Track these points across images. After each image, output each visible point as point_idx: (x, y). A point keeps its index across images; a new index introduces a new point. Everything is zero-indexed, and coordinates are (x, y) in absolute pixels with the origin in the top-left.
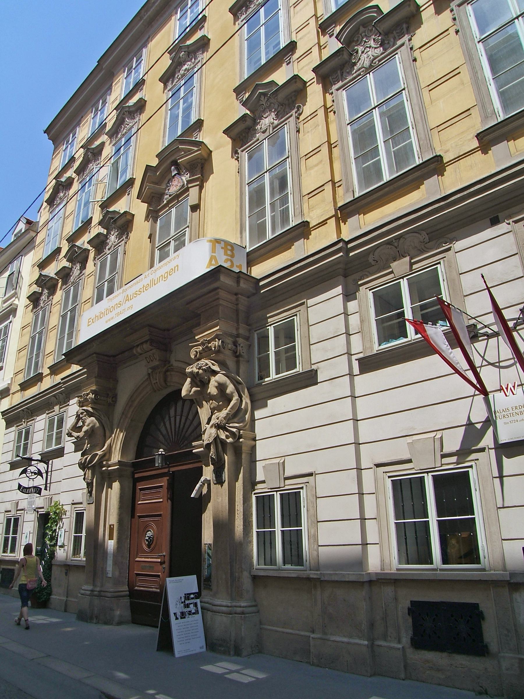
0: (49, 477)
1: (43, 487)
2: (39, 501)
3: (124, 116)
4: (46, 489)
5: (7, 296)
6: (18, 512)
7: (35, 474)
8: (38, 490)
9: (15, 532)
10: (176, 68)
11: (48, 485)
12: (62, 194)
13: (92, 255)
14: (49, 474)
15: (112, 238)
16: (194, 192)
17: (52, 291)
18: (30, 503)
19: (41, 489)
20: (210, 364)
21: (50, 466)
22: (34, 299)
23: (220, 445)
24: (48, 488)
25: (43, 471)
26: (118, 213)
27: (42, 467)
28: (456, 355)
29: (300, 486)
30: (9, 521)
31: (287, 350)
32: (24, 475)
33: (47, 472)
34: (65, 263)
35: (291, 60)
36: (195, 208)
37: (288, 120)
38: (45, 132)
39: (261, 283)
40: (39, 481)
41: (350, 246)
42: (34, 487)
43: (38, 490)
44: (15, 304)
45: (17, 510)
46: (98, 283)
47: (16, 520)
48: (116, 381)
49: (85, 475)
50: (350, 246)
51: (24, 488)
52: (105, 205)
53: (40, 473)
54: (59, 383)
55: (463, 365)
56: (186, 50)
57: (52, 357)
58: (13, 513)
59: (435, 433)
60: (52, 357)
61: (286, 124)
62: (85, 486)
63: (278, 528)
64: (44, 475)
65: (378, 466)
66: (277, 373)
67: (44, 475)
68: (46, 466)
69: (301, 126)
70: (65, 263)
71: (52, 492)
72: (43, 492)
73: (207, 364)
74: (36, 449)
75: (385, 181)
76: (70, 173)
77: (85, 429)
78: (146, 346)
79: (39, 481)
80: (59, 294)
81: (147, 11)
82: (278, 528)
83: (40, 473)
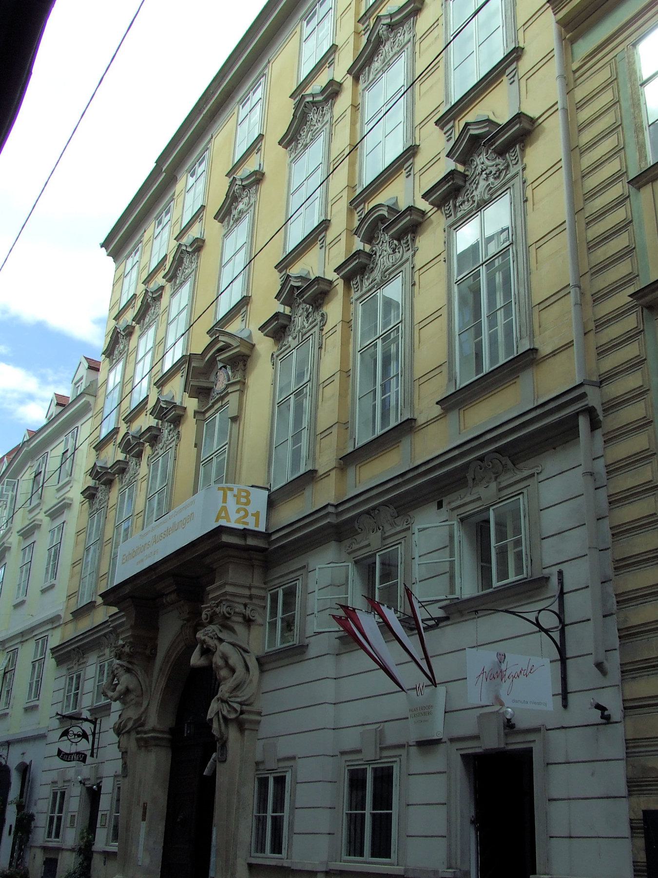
0: (96, 740)
1: (88, 753)
2: (85, 771)
3: (182, 256)
4: (92, 755)
5: (60, 485)
6: (386, 753)
7: (79, 736)
8: (82, 757)
10: (231, 204)
11: (95, 751)
14: (97, 736)
15: (299, 321)
16: (233, 399)
17: (109, 483)
18: (78, 773)
19: (86, 756)
20: (217, 632)
21: (98, 726)
22: (90, 494)
23: (222, 721)
25: (89, 732)
26: (307, 279)
27: (87, 727)
28: (412, 643)
29: (394, 759)
32: (65, 738)
33: (94, 734)
34: (152, 421)
35: (412, 172)
36: (235, 419)
37: (512, 182)
39: (274, 537)
40: (84, 746)
42: (78, 753)
43: (82, 757)
44: (68, 499)
45: (382, 749)
46: (458, 275)
47: (63, 794)
48: (156, 629)
49: (119, 742)
51: (66, 754)
52: (283, 265)
53: (84, 735)
54: (107, 621)
55: (418, 654)
56: (388, 21)
57: (105, 581)
58: (60, 785)
59: (378, 725)
60: (105, 581)
61: (509, 188)
62: (120, 755)
63: (368, 811)
64: (91, 738)
65: (343, 753)
66: (282, 642)
67: (91, 738)
68: (92, 726)
69: (529, 193)
70: (152, 421)
71: (99, 760)
73: (214, 631)
74: (87, 701)
76: (159, 280)
77: (118, 688)
78: (173, 597)
79: (84, 746)
80: (114, 493)
81: (206, 103)
82: (368, 811)
83: (84, 735)
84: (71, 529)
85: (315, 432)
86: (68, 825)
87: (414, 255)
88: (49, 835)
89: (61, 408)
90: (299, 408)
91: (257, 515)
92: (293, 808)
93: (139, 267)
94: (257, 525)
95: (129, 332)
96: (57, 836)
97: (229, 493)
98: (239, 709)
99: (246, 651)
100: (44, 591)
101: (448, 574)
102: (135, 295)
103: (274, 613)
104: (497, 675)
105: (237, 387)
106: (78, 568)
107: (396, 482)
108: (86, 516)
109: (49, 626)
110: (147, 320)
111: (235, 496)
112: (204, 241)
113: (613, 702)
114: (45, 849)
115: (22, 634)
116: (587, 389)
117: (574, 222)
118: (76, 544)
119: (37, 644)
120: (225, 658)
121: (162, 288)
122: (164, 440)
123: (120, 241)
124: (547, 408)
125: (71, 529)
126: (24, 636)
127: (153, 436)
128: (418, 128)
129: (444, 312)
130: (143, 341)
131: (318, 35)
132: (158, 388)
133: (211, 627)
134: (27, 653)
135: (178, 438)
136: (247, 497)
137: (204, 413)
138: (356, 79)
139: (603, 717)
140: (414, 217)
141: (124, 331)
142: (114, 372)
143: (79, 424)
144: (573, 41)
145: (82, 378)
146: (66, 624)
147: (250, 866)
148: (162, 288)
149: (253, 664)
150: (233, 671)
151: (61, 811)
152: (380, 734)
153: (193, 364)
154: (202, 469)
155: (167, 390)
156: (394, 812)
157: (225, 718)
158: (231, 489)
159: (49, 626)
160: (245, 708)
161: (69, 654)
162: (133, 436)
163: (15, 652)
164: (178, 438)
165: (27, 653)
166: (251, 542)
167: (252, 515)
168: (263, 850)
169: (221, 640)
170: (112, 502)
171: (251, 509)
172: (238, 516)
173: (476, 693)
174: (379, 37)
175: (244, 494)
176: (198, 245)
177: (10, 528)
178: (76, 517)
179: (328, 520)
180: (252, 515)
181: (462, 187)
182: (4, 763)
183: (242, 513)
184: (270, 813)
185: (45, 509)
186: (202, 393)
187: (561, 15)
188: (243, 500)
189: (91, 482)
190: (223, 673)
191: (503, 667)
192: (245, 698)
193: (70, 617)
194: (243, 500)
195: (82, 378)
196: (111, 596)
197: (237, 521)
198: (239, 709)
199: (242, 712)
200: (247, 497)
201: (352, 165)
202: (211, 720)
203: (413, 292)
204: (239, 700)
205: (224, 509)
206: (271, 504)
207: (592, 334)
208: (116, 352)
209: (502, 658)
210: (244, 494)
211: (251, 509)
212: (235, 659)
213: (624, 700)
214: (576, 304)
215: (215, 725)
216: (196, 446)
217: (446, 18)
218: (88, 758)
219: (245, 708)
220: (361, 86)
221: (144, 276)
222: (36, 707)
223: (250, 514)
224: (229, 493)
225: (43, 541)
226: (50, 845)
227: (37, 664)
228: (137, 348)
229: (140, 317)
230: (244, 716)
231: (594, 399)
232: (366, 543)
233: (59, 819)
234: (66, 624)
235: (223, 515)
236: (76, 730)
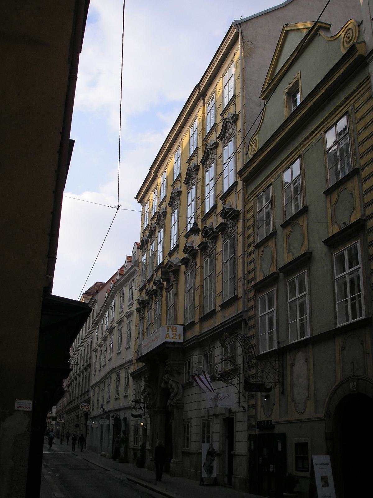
6: (210, 418)
7: (139, 408)
9: (209, 432)
10: (173, 201)
11: (145, 414)
12: (231, 130)
13: (199, 253)
17: (215, 239)
22: (138, 310)
23: (171, 406)
24: (145, 415)
25: (142, 407)
30: (204, 423)
31: (271, 336)
34: (221, 220)
38: (135, 199)
41: (199, 337)
44: (132, 311)
45: (209, 416)
50: (199, 337)
51: (134, 415)
53: (141, 408)
58: (206, 418)
70: (221, 220)
72: (143, 417)
75: (257, 282)
80: (220, 245)
84: (134, 324)
85: (237, 278)
86: (140, 441)
87: (216, 248)
88: (134, 444)
89: (121, 276)
90: (211, 281)
91: (179, 335)
92: (191, 434)
93: (216, 107)
94: (180, 338)
95: (215, 146)
96: (188, 447)
97: (169, 328)
98: (176, 402)
99: (178, 383)
100: (127, 349)
101: (242, 356)
102: (215, 124)
103: (186, 371)
104: (216, 398)
105: (175, 282)
106: (137, 341)
107: (233, 319)
108: (138, 318)
109: (129, 364)
110: (208, 162)
111: (171, 329)
112: (167, 212)
113: (245, 405)
114: (133, 449)
115: (121, 366)
116: (243, 314)
117: (244, 254)
118: (136, 330)
119: (126, 370)
120: (171, 386)
121: (155, 227)
122: (159, 295)
123: (141, 197)
124: (203, 335)
125: (134, 324)
126: (122, 366)
127: (222, 228)
128: (217, 197)
129: (222, 272)
130: (226, 150)
131: (194, 137)
132: (222, 201)
133: (167, 375)
134: (123, 374)
135: (162, 296)
136: (176, 329)
137: (168, 289)
138: (203, 165)
139: (244, 410)
140: (215, 234)
141: (194, 168)
142: (227, 147)
143: (133, 278)
144: (247, 186)
145: (135, 253)
146: (135, 363)
147: (183, 452)
148: (155, 227)
149: (180, 387)
150: (174, 389)
151: (184, 437)
152: (208, 411)
153: (163, 270)
154: (168, 311)
155: (227, 202)
156: (210, 435)
157: (173, 406)
158: (170, 327)
159: (129, 364)
160: (178, 402)
161: (136, 376)
162: (209, 228)
163: (119, 373)
164: (162, 296)
165: (123, 374)
166: (177, 346)
167: (178, 335)
168: (184, 447)
169: (170, 380)
170: (146, 315)
171: (177, 333)
172: (173, 336)
173: (209, 404)
174: (208, 152)
175: (174, 328)
176: (179, 193)
177: (122, 311)
178: (135, 318)
179: (195, 341)
180: (178, 335)
181: (206, 247)
182: (119, 417)
183: (174, 335)
184: (186, 436)
185: (115, 321)
186: (168, 280)
187: (242, 178)
188: (174, 330)
189: (139, 306)
190: (171, 390)
191: (219, 396)
192: (178, 399)
193: (135, 361)
194: (174, 330)
195: (135, 253)
196: (140, 360)
197: (173, 338)
198: (176, 402)
199: (177, 403)
200: (176, 329)
201: (196, 209)
202: (168, 406)
203: (216, 262)
204: (176, 399)
205: (168, 334)
206: (185, 331)
207: (247, 294)
208: (227, 135)
209: (218, 394)
210: (174, 328)
211: (177, 333)
212: (174, 386)
213: (249, 405)
214: (243, 284)
215: (169, 407)
216: (166, 301)
217: (223, 154)
218: (143, 416)
219: (178, 402)
220: (205, 169)
221: (221, 111)
222: (118, 398)
223: (177, 335)
224: (169, 328)
225: (125, 326)
226: (135, 447)
227: (127, 378)
228: (222, 155)
229: (204, 161)
230: (178, 405)
231: (245, 316)
232: (213, 346)
233: (137, 438)
234: (135, 363)
235: (168, 336)
236: (137, 406)
